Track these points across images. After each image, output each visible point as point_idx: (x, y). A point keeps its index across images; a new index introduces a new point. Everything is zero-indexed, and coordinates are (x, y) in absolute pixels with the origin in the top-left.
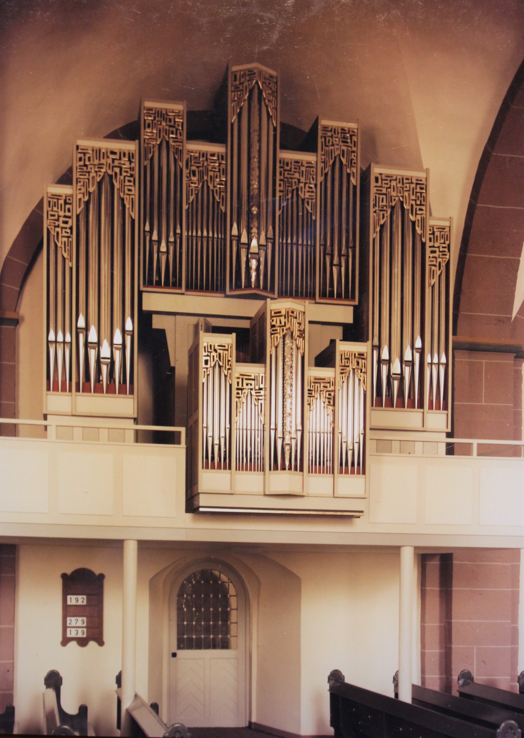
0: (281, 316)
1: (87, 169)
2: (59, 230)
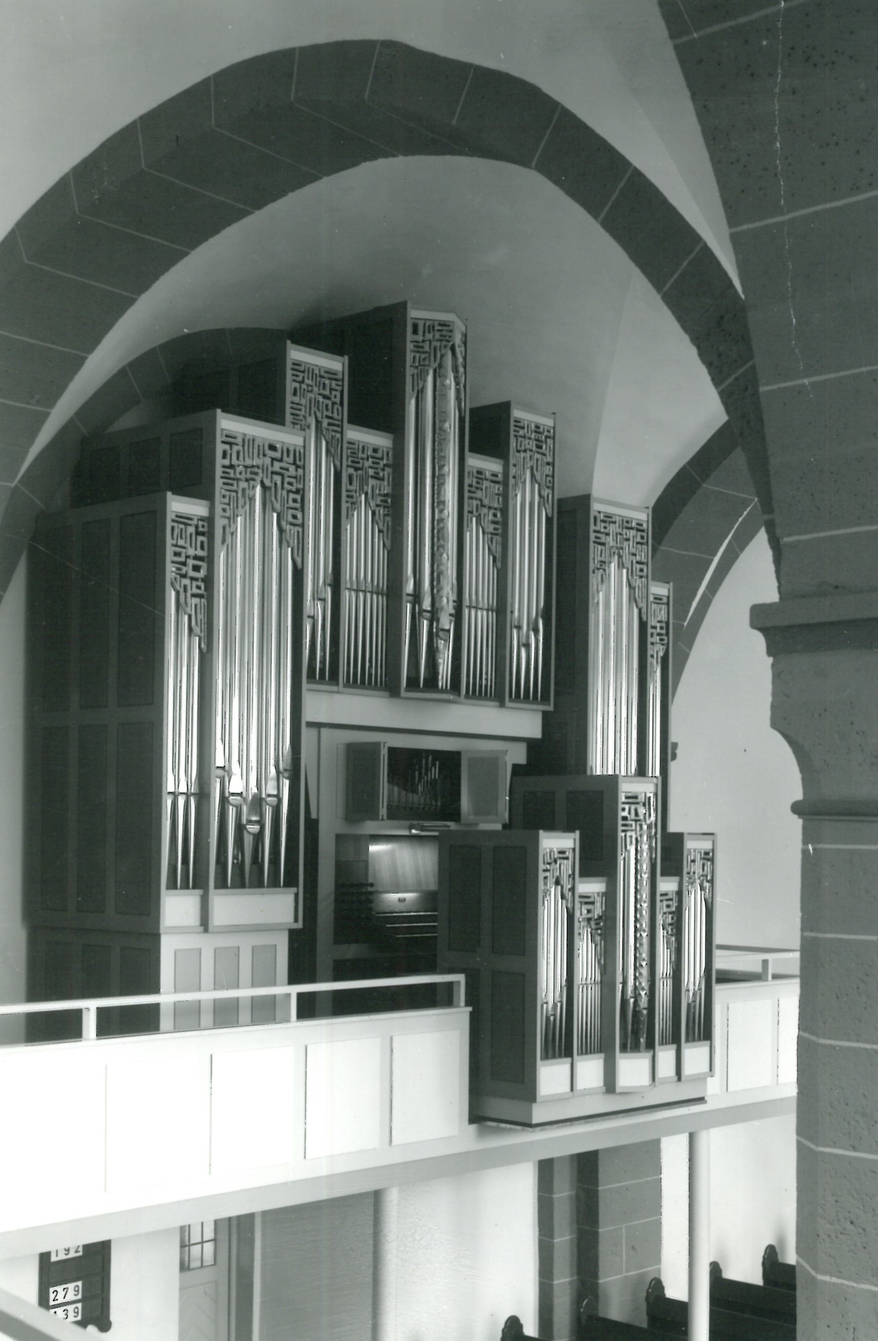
0: (638, 803)
1: (235, 473)
2: (186, 581)
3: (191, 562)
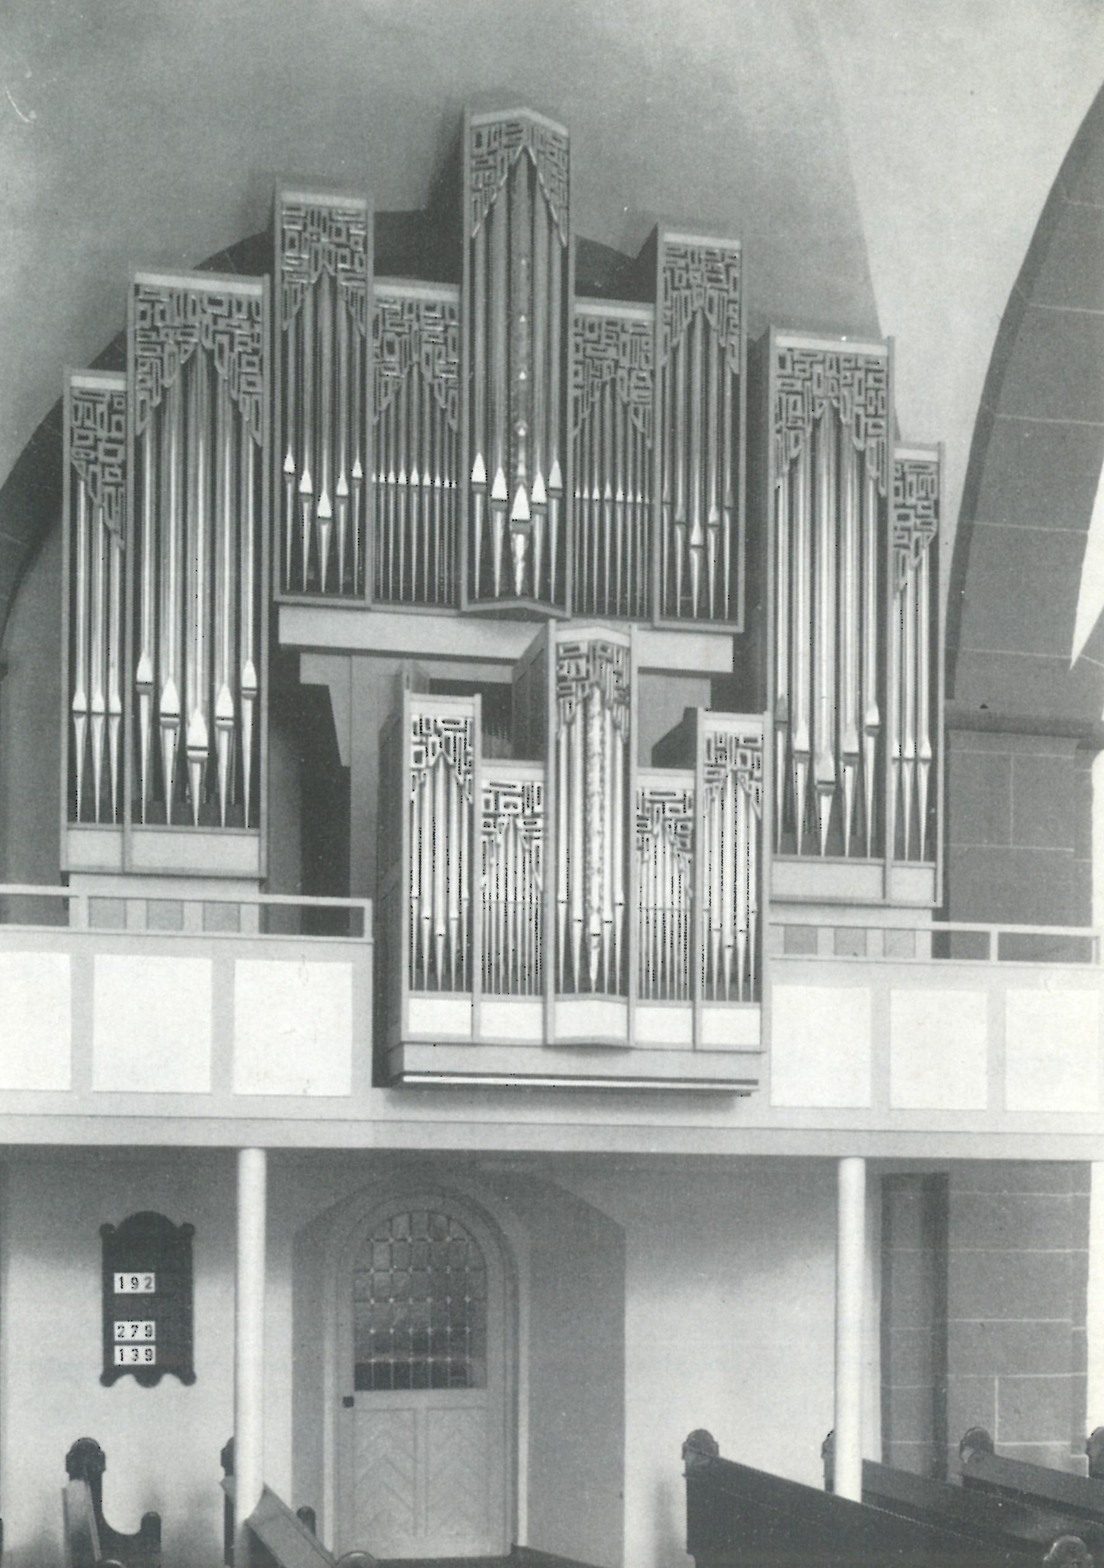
2: (96, 469)
3: (102, 446)
